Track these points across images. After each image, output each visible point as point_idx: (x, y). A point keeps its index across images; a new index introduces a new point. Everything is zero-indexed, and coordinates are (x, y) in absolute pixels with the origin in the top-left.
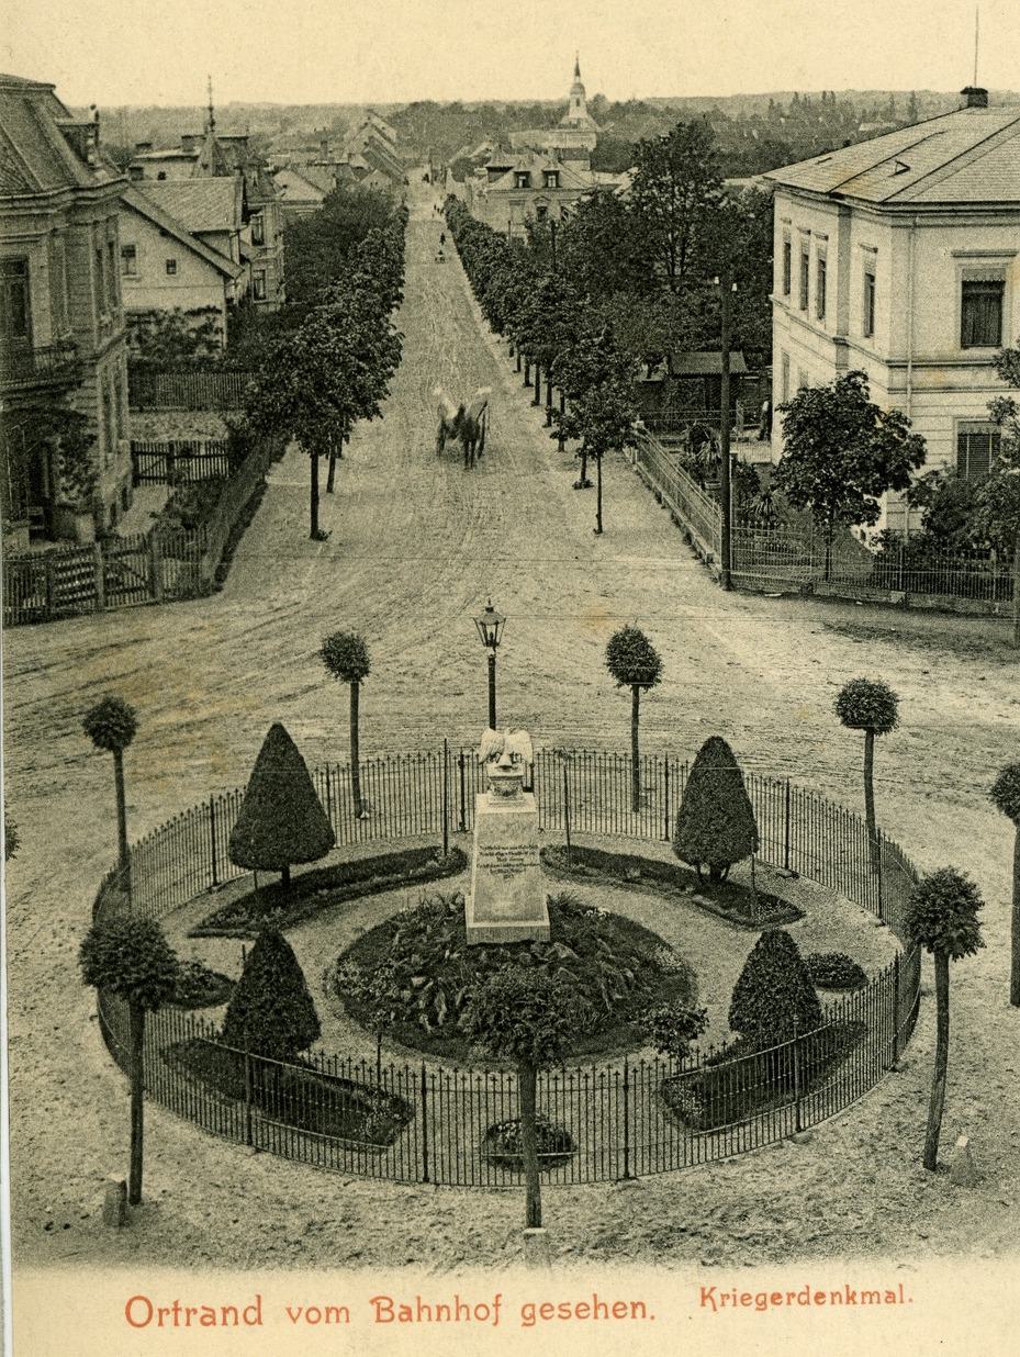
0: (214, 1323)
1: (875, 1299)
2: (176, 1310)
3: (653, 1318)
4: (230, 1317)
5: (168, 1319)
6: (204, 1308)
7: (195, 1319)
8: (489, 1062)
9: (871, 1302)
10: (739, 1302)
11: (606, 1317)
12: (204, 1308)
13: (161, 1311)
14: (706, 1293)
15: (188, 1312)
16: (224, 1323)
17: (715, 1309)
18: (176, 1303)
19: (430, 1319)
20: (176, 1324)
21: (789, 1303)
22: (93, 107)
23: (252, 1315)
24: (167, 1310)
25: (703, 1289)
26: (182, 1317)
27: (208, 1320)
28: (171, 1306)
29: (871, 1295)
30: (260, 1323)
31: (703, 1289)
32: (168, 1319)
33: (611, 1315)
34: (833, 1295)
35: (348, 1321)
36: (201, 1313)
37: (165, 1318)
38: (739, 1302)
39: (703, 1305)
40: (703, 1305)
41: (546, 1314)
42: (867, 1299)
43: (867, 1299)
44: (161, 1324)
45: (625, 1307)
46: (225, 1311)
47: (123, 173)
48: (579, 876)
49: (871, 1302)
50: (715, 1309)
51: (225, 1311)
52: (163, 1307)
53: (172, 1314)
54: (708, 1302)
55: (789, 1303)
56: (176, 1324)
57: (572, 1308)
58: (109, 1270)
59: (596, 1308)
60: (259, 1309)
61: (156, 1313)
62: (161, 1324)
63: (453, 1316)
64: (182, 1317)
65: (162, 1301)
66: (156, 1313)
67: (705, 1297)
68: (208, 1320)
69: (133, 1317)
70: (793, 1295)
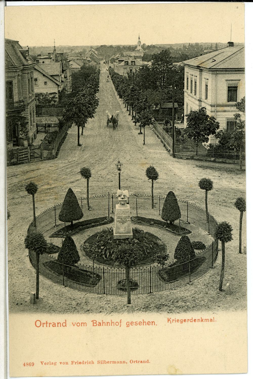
0: (55, 326)
1: (208, 321)
2: (47, 323)
4: (59, 325)
5: (45, 325)
6: (53, 323)
7: (51, 325)
12: (53, 323)
13: (43, 323)
14: (169, 319)
15: (49, 324)
16: (58, 326)
17: (171, 323)
18: (47, 322)
19: (105, 325)
20: (47, 326)
23: (64, 324)
26: (48, 325)
27: (54, 325)
28: (45, 322)
30: (66, 326)
32: (45, 325)
34: (198, 320)
35: (86, 326)
36: (52, 324)
37: (173, 321)
39: (168, 322)
40: (168, 322)
44: (43, 326)
45: (150, 323)
46: (58, 323)
48: (140, 223)
50: (171, 323)
51: (58, 323)
54: (169, 321)
55: (188, 322)
56: (47, 326)
59: (143, 323)
61: (42, 324)
62: (43, 326)
64: (48, 325)
65: (43, 321)
66: (42, 324)
67: (169, 320)
68: (54, 325)
70: (189, 320)
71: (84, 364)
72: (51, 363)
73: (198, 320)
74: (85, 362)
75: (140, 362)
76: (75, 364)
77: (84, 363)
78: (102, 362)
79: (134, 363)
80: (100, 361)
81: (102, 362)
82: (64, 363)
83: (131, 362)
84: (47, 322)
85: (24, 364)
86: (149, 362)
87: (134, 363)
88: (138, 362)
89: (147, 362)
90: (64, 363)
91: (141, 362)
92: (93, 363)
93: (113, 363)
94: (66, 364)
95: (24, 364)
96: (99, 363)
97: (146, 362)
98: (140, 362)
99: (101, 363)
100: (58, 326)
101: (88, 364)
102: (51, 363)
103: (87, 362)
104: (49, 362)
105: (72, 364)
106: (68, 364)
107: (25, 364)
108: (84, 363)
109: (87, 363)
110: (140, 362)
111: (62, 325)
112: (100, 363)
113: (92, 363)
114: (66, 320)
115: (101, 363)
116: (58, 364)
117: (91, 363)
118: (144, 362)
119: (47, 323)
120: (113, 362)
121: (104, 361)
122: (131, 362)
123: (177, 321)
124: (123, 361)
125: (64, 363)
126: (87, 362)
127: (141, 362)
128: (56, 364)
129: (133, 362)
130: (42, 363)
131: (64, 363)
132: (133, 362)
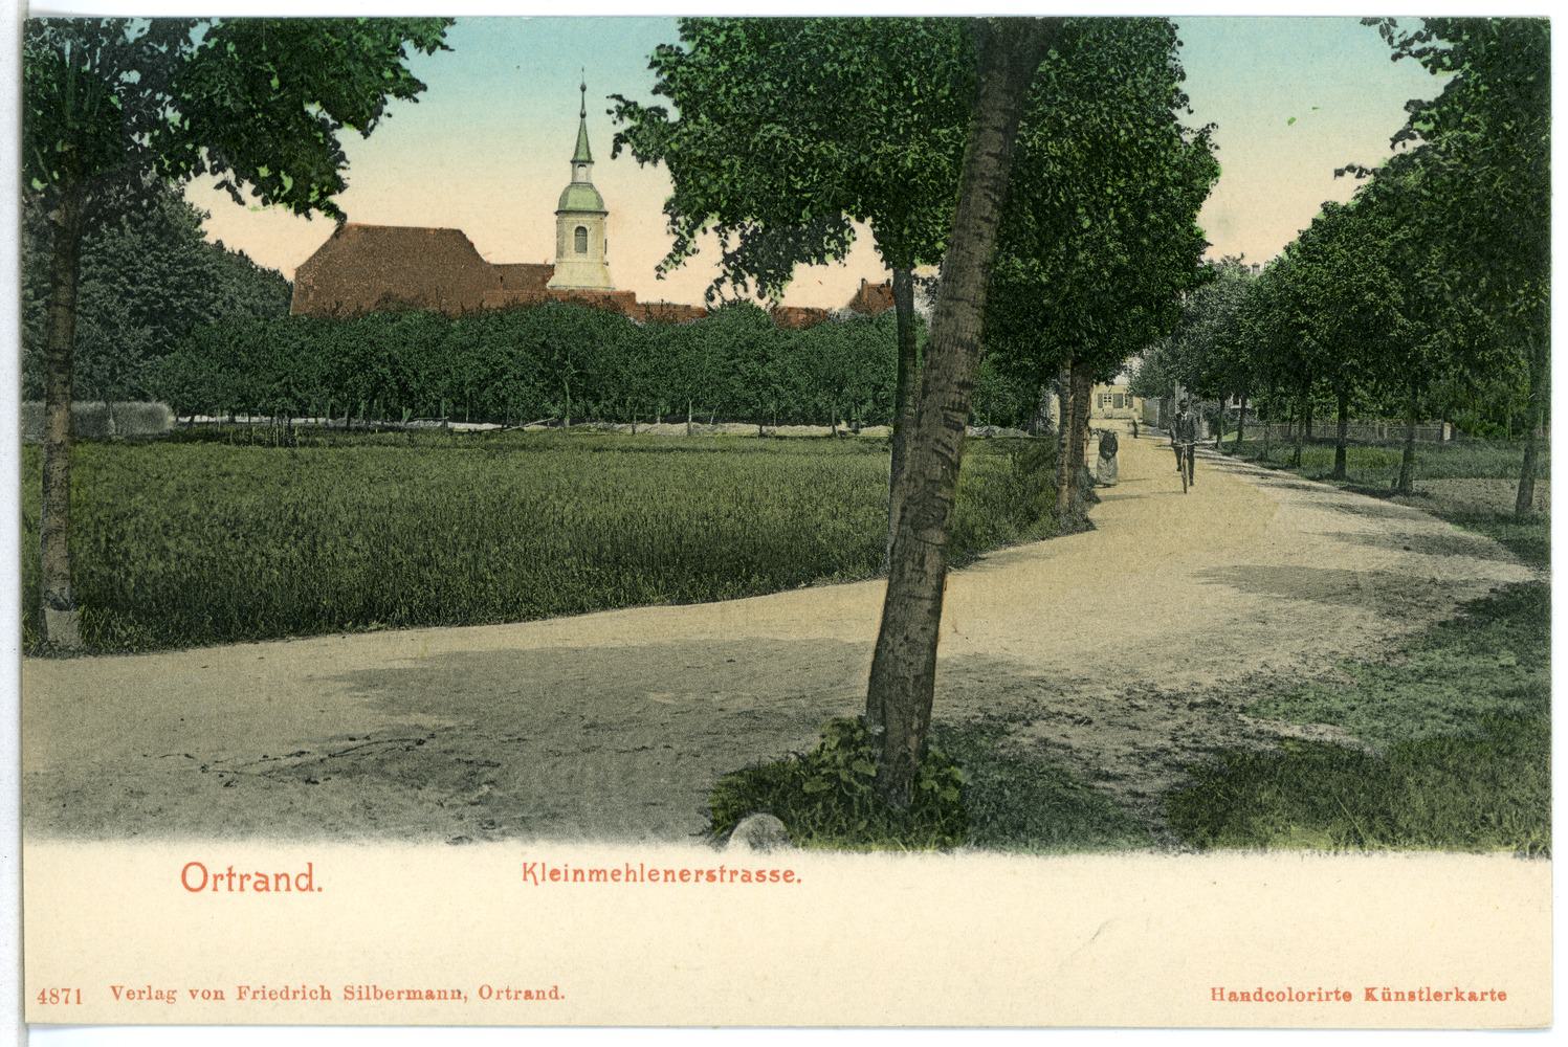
0: (267, 889)
1: (602, 876)
2: (231, 875)
3: (799, 881)
4: (283, 882)
5: (223, 884)
6: (257, 874)
7: (248, 885)
8: (782, 764)
9: (598, 880)
10: (609, 877)
11: (288, 889)
12: (257, 874)
13: (215, 877)
14: (529, 867)
15: (242, 877)
16: (277, 889)
17: (536, 884)
18: (230, 869)
20: (230, 889)
21: (697, 880)
22: (854, 239)
23: (303, 882)
24: (222, 877)
25: (525, 864)
26: (236, 882)
27: (260, 886)
28: (225, 872)
29: (599, 873)
31: (525, 864)
32: (223, 884)
33: (293, 886)
34: (667, 873)
36: (255, 878)
37: (700, 877)
38: (609, 877)
39: (525, 879)
40: (525, 879)
41: (653, 877)
42: (594, 876)
43: (594, 876)
44: (215, 889)
46: (278, 877)
47: (681, 80)
49: (598, 880)
50: (536, 884)
51: (278, 877)
52: (218, 873)
53: (226, 879)
55: (697, 880)
56: (230, 889)
57: (781, 874)
58: (555, 844)
60: (310, 876)
61: (211, 880)
62: (215, 889)
63: (639, 878)
64: (236, 882)
65: (217, 866)
66: (211, 880)
67: (527, 871)
68: (260, 886)
69: (199, 869)
70: (701, 872)
71: (287, 998)
72: (153, 994)
73: (667, 873)
74: (1327, 994)
75: (404, 996)
76: (254, 997)
77: (291, 995)
78: (364, 990)
79: (498, 998)
80: (356, 989)
81: (364, 990)
82: (206, 995)
83: (486, 992)
84: (230, 869)
85: (43, 993)
86: (559, 995)
87: (498, 998)
88: (512, 994)
89: (553, 994)
90: (206, 995)
91: (528, 995)
92: (325, 994)
93: (409, 998)
94: (216, 998)
95: (43, 993)
96: (350, 996)
97: (547, 995)
98: (523, 995)
99: (360, 998)
100: (277, 889)
101: (304, 998)
102: (153, 994)
103: (301, 989)
104: (147, 990)
105: (241, 998)
106: (222, 998)
107: (48, 995)
108: (291, 995)
109: (1317, 996)
110: (404, 996)
111: (293, 886)
112: (357, 995)
113: (323, 998)
114: (310, 865)
115: (360, 998)
116: (337, 992)
117: (319, 994)
118: (442, 995)
119: (231, 875)
120: (409, 992)
121: (372, 991)
122: (486, 992)
123: (650, 875)
124: (538, 992)
125: (206, 995)
126: (1316, 991)
127: (528, 995)
128: (175, 995)
129: (494, 994)
130: (118, 990)
131: (206, 995)
132: (494, 994)
